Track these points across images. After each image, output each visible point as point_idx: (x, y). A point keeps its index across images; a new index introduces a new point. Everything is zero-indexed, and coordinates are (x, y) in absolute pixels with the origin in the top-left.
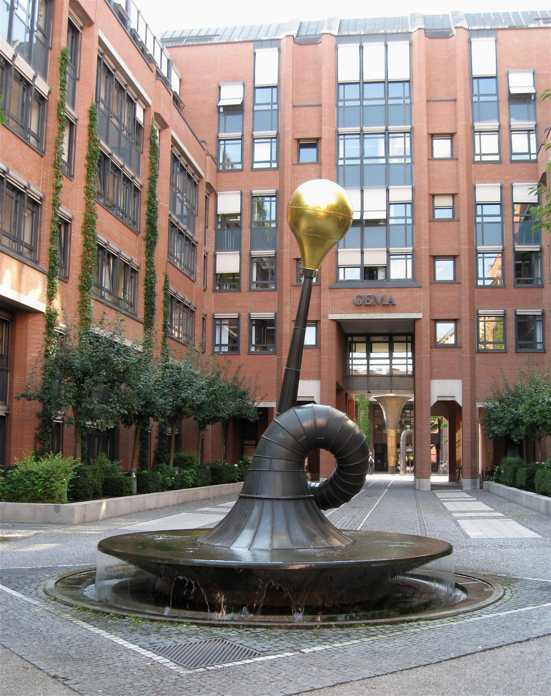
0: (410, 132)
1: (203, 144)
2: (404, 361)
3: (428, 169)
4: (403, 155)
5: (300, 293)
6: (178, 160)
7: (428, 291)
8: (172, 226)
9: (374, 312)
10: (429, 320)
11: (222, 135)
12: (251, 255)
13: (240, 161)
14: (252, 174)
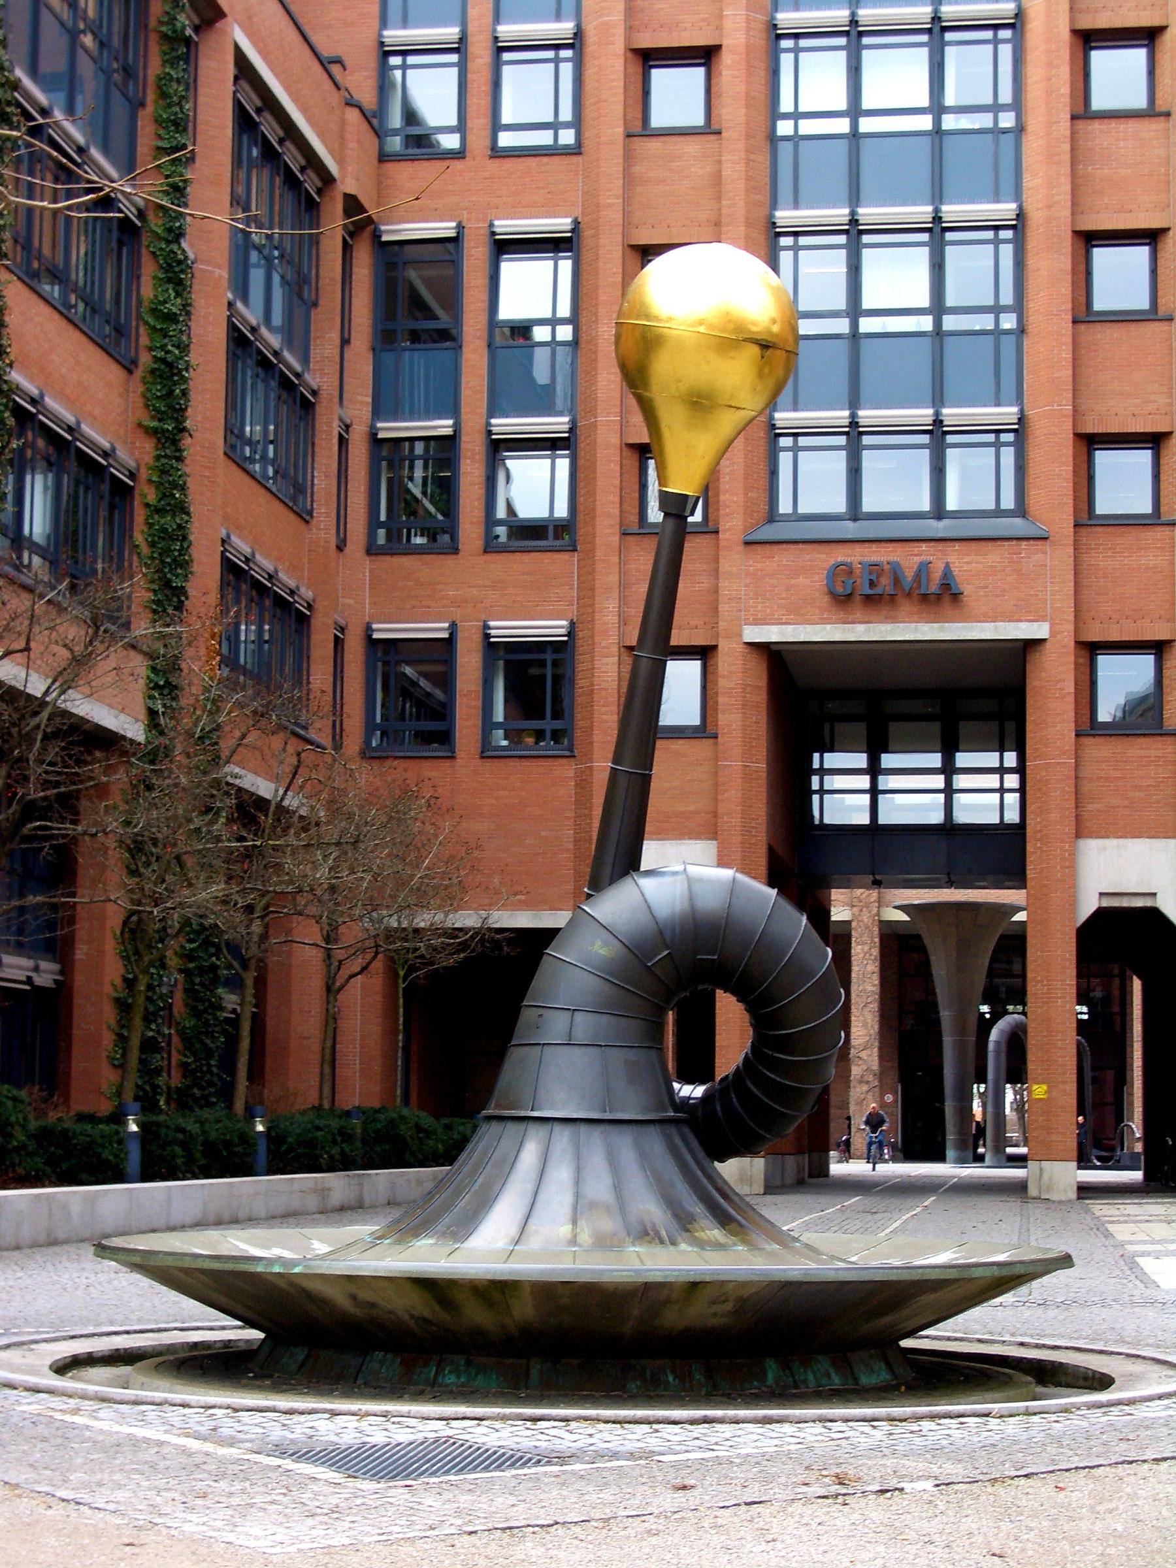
0: (1011, 26)
1: (336, 70)
2: (993, 781)
3: (1073, 149)
4: (997, 765)
5: (652, 559)
6: (261, 127)
7: (1071, 550)
8: (240, 342)
9: (892, 619)
10: (1069, 234)
11: (395, 35)
12: (490, 433)
13: (453, 121)
14: (494, 166)
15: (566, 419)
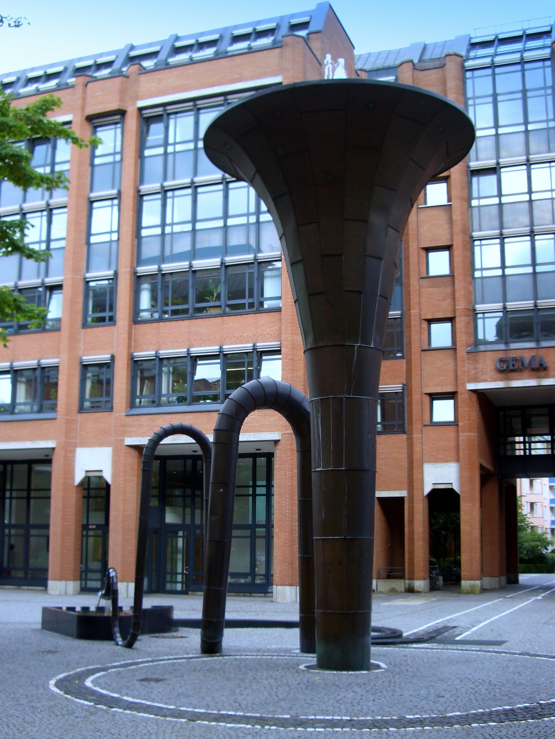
15: (400, 312)
